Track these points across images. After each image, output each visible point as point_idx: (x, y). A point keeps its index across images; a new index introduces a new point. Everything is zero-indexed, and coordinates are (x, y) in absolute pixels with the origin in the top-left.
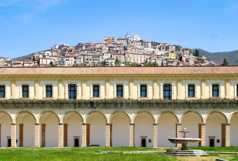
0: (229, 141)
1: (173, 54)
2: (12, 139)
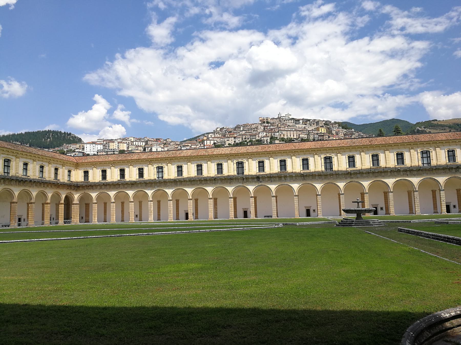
0: (393, 208)
1: (323, 129)
2: (189, 212)
